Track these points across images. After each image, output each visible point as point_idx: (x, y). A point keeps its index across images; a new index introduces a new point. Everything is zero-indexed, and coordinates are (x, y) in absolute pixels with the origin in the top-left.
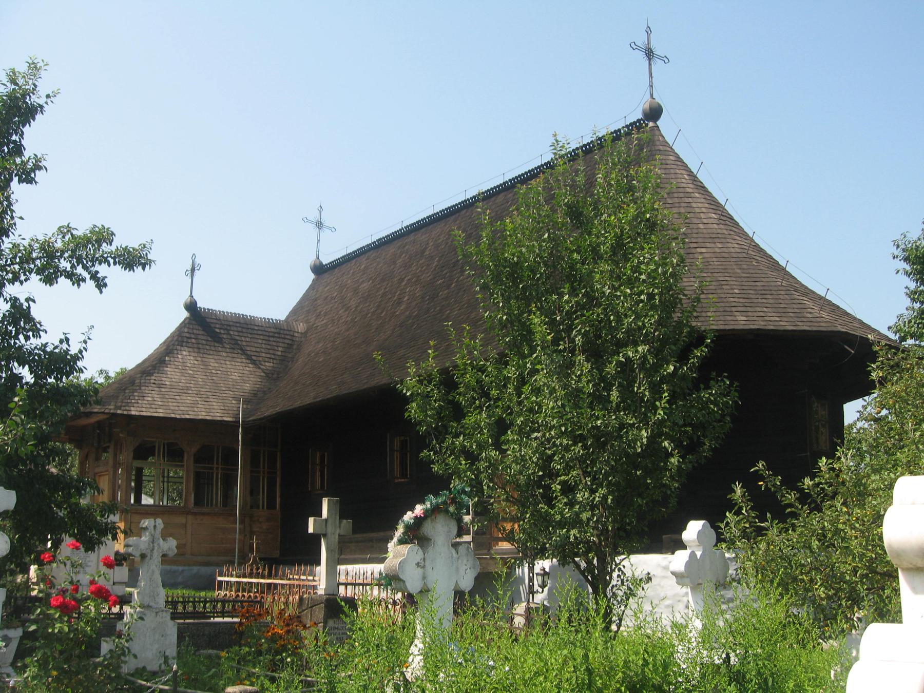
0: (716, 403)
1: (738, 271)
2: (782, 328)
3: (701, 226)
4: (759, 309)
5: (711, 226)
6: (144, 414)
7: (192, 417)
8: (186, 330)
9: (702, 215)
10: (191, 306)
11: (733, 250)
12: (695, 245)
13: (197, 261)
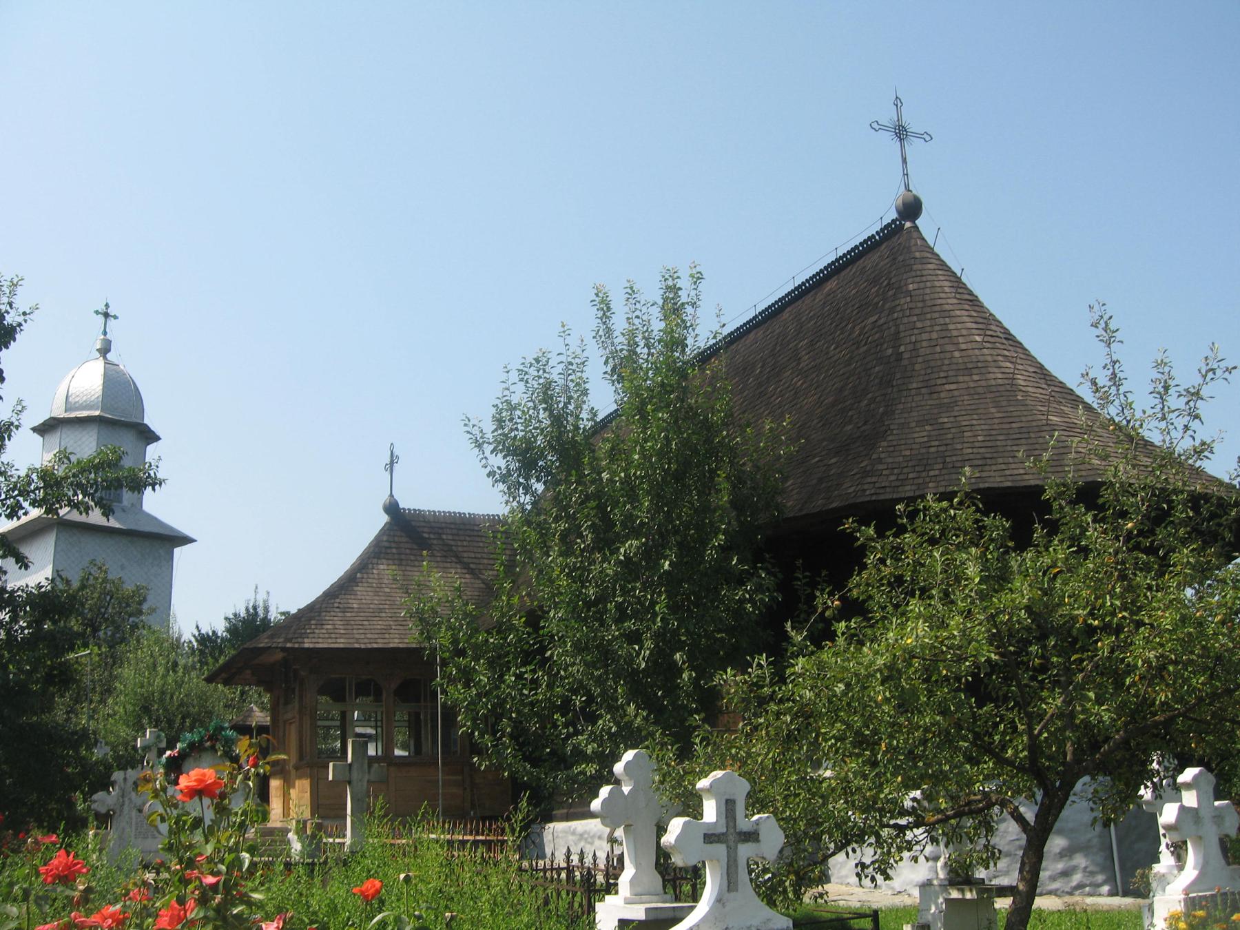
0: (751, 600)
1: (993, 410)
3: (957, 354)
4: (1001, 460)
5: (970, 352)
6: (321, 646)
7: (380, 646)
8: (385, 538)
9: (961, 340)
10: (392, 508)
11: (993, 382)
12: (944, 381)
13: (396, 452)
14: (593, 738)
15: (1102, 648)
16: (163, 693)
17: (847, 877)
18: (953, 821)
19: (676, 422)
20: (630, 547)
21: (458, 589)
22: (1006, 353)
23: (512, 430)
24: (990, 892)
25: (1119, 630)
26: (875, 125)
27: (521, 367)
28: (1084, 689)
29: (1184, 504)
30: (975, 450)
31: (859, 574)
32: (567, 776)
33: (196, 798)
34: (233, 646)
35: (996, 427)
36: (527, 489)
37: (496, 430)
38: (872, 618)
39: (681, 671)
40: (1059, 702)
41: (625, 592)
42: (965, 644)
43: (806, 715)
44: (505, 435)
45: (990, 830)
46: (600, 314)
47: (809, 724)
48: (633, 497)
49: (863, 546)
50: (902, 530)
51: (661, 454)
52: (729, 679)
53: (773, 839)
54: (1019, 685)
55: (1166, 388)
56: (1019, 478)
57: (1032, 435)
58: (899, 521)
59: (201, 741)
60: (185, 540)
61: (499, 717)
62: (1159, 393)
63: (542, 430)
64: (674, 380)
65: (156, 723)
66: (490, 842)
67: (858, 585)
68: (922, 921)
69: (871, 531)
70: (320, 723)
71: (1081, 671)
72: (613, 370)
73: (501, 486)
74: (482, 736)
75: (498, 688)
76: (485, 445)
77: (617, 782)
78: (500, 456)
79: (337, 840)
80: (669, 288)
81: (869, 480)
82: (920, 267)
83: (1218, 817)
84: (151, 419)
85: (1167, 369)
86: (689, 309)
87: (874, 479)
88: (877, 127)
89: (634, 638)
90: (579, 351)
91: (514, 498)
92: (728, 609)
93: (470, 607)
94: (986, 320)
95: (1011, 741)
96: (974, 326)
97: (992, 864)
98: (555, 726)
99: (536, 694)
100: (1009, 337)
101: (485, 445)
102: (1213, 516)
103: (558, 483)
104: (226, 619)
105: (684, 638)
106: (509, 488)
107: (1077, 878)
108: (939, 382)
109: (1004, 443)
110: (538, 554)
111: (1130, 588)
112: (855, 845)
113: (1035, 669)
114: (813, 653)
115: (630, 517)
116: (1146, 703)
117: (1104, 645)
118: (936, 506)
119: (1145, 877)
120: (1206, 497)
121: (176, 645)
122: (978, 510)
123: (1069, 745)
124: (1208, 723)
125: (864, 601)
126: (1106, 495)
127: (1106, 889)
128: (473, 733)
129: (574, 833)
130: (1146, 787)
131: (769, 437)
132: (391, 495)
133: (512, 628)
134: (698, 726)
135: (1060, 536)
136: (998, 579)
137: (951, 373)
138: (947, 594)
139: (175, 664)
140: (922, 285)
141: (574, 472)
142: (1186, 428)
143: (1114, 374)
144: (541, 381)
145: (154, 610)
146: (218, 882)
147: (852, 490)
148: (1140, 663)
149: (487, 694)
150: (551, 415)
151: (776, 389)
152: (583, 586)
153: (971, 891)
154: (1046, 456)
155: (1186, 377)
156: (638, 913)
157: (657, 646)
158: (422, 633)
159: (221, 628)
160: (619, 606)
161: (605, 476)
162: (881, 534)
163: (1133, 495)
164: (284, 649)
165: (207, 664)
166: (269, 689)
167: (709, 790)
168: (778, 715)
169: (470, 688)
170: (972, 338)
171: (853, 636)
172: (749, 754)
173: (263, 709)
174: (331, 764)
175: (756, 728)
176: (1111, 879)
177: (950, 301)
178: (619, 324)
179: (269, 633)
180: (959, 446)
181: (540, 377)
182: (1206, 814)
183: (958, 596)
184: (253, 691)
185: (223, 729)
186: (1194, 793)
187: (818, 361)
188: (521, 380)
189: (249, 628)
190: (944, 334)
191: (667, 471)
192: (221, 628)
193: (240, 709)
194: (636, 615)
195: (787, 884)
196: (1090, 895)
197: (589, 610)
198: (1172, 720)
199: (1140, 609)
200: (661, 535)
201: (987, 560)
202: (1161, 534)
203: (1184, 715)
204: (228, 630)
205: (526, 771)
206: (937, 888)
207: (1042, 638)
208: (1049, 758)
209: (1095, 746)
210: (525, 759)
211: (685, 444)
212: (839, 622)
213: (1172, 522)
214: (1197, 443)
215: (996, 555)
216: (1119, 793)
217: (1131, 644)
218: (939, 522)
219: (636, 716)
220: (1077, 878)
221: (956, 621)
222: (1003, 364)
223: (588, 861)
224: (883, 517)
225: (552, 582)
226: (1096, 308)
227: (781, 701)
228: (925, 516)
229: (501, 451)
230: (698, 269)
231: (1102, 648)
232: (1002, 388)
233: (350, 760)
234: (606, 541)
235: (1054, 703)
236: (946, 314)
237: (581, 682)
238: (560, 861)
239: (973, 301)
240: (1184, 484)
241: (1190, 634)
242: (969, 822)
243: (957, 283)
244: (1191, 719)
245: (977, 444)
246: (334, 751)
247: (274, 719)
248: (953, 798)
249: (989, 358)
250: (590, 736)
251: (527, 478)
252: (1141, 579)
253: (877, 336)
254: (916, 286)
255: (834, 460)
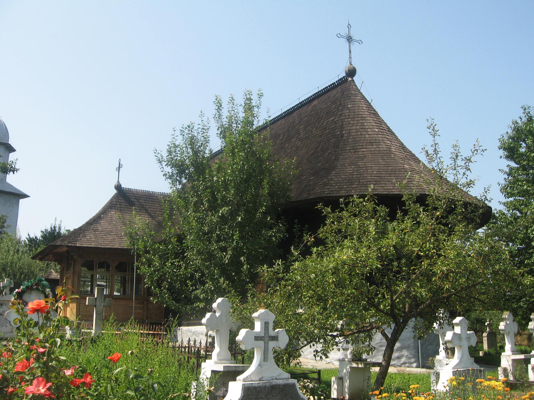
0: (275, 236)
1: (381, 161)
2: (392, 193)
3: (367, 136)
4: (383, 182)
5: (373, 136)
6: (84, 245)
7: (110, 247)
8: (114, 200)
9: (369, 130)
11: (382, 149)
12: (361, 147)
13: (121, 163)
14: (204, 291)
15: (424, 265)
16: (12, 263)
17: (307, 355)
18: (356, 335)
19: (247, 157)
20: (224, 210)
21: (147, 224)
22: (388, 137)
23: (175, 156)
24: (369, 365)
25: (432, 257)
26: (339, 35)
27: (182, 129)
28: (415, 281)
29: (461, 206)
30: (372, 178)
31: (323, 227)
32: (192, 307)
33: (36, 313)
34: (44, 243)
35: (382, 168)
36: (180, 182)
37: (168, 156)
38: (327, 247)
39: (243, 265)
40: (405, 286)
41: (221, 229)
42: (367, 259)
43: (297, 286)
44: (172, 158)
45: (371, 339)
46: (217, 108)
47: (298, 291)
48: (226, 189)
49: (326, 216)
50: (342, 210)
51: (240, 171)
52: (264, 270)
53: (283, 340)
54: (388, 279)
55: (457, 156)
56: (390, 190)
57: (397, 173)
58: (341, 205)
59: (32, 286)
60: (25, 196)
61: (163, 281)
62: (454, 158)
63: (189, 157)
64: (247, 139)
65: (8, 276)
66: (155, 334)
67: (322, 232)
68: (340, 376)
69: (329, 210)
70: (82, 279)
71: (415, 274)
72: (221, 133)
73: (169, 181)
74: (155, 288)
75: (163, 268)
76: (163, 162)
77: (215, 312)
78: (169, 167)
79: (89, 331)
80: (247, 99)
81: (327, 187)
82: (354, 98)
83: (469, 338)
84: (12, 142)
85: (457, 149)
86: (256, 109)
87: (329, 187)
88: (340, 36)
89: (224, 249)
90: (206, 124)
91: (174, 186)
92: (265, 239)
93: (153, 233)
94: (380, 122)
95: (382, 302)
96: (375, 124)
97: (371, 353)
98: (187, 286)
99: (179, 271)
100: (389, 130)
101: (163, 162)
102: (473, 212)
103: (194, 181)
104: (41, 231)
105: (245, 251)
106: (172, 182)
107: (403, 360)
108: (359, 147)
109: (385, 175)
110: (183, 211)
111: (437, 240)
112: (314, 343)
113: (394, 272)
114: (302, 260)
115: (224, 197)
116: (441, 288)
117: (425, 263)
118: (358, 201)
119: (433, 361)
120: (470, 204)
121: (19, 242)
122: (375, 203)
123: (407, 305)
124: (465, 298)
125: (324, 239)
126: (429, 201)
127: (415, 365)
128: (151, 287)
129: (190, 332)
130: (437, 323)
131: (286, 166)
132: (118, 182)
133: (170, 242)
134: (250, 289)
135: (408, 216)
136: (382, 233)
137: (364, 144)
138: (359, 238)
139: (18, 250)
140: (354, 105)
141: (201, 176)
142: (464, 174)
143: (435, 149)
144: (190, 135)
145: (9, 226)
146: (45, 351)
147: (320, 191)
148: (439, 272)
149: (158, 270)
150: (193, 150)
151: (288, 146)
152: (202, 226)
153: (361, 364)
154: (405, 182)
155: (465, 152)
156: (220, 368)
157: (233, 253)
158: (131, 243)
159: (39, 235)
160: (218, 236)
161: (215, 179)
162: (333, 211)
163: (440, 201)
164: (67, 246)
165: (32, 251)
166: (60, 263)
167: (257, 318)
168: (285, 286)
169: (150, 267)
170: (374, 129)
171: (319, 254)
172: (272, 302)
173: (56, 272)
174: (87, 298)
175: (275, 291)
176: (417, 361)
177: (365, 113)
178: (225, 113)
179: (61, 239)
180: (365, 175)
181: (189, 134)
182: (464, 336)
183: (364, 239)
184: (52, 264)
185: (42, 280)
186: (459, 327)
187: (308, 135)
188: (181, 134)
189: (52, 236)
190: (362, 127)
191: (242, 178)
192: (39, 235)
193: (46, 272)
194: (225, 240)
195: (285, 358)
196: (408, 367)
197: (204, 236)
198: (450, 296)
199: (440, 249)
200: (238, 206)
201: (378, 225)
202: (450, 218)
203: (455, 295)
204: (42, 237)
205: (174, 305)
206: (347, 362)
207: (399, 259)
208: (399, 310)
209: (417, 306)
210: (173, 299)
211: (250, 167)
212: (314, 247)
213: (456, 213)
214: (468, 181)
215: (381, 223)
216: (426, 325)
217: (435, 264)
218: (359, 207)
219: (223, 283)
220: (403, 360)
221: (363, 250)
222: (386, 142)
223: (198, 345)
224: (334, 203)
225: (189, 223)
226: (430, 120)
227: (287, 280)
228: (353, 204)
229: (170, 165)
230: (261, 92)
231: (424, 265)
232: (386, 152)
233: (96, 296)
234: (214, 207)
235: (402, 287)
236: (364, 119)
237: (199, 267)
238: (185, 344)
239: (375, 114)
240: (462, 198)
241: (460, 261)
242: (362, 335)
243: (369, 106)
244: (458, 296)
245: (373, 175)
246: (87, 291)
247: (62, 277)
248: (357, 325)
249: (381, 139)
250: (202, 291)
251: (181, 178)
252: (442, 237)
253: (333, 126)
254: (351, 106)
255: (312, 178)
